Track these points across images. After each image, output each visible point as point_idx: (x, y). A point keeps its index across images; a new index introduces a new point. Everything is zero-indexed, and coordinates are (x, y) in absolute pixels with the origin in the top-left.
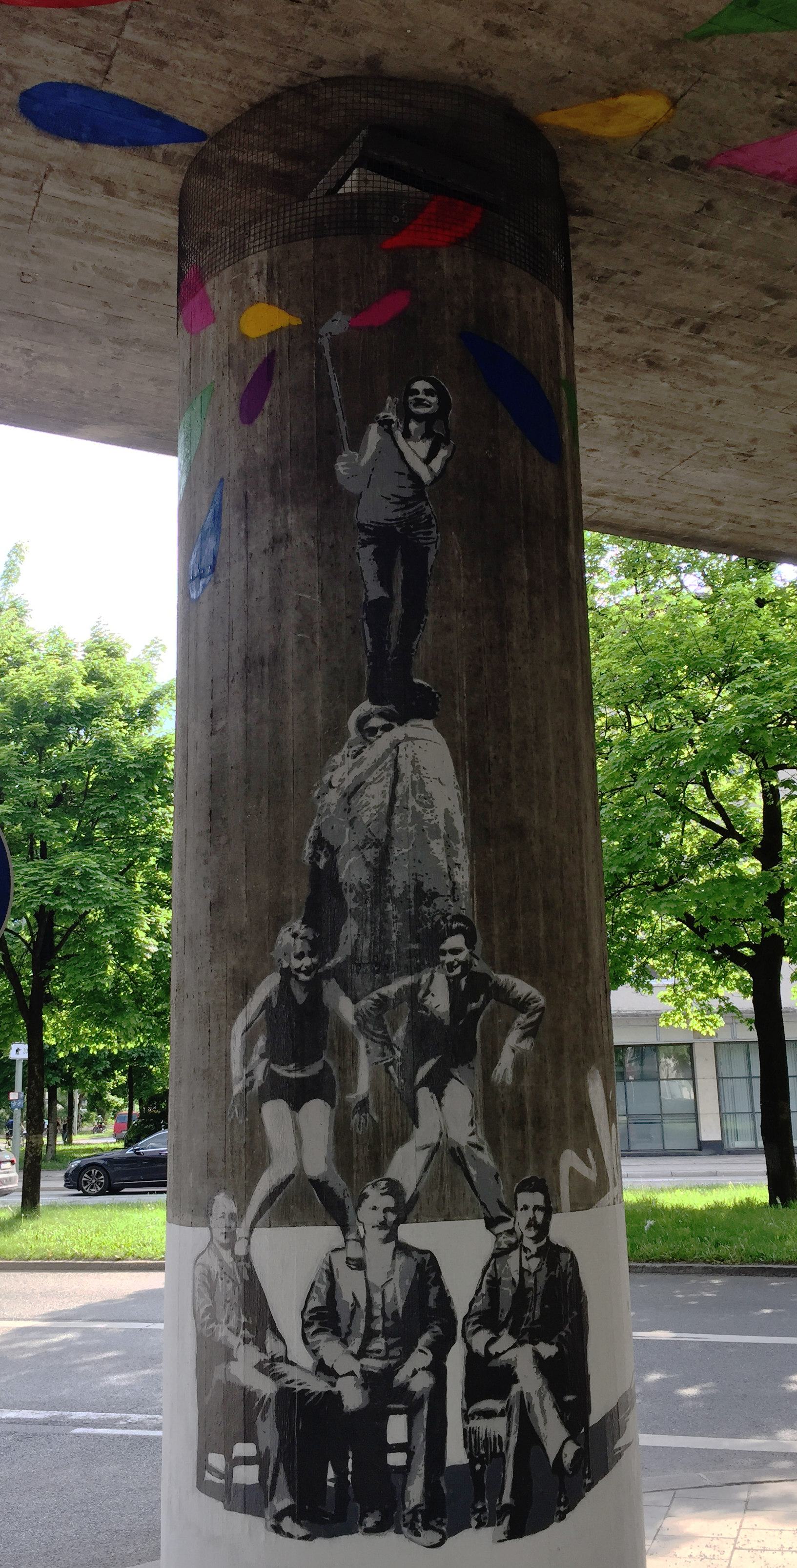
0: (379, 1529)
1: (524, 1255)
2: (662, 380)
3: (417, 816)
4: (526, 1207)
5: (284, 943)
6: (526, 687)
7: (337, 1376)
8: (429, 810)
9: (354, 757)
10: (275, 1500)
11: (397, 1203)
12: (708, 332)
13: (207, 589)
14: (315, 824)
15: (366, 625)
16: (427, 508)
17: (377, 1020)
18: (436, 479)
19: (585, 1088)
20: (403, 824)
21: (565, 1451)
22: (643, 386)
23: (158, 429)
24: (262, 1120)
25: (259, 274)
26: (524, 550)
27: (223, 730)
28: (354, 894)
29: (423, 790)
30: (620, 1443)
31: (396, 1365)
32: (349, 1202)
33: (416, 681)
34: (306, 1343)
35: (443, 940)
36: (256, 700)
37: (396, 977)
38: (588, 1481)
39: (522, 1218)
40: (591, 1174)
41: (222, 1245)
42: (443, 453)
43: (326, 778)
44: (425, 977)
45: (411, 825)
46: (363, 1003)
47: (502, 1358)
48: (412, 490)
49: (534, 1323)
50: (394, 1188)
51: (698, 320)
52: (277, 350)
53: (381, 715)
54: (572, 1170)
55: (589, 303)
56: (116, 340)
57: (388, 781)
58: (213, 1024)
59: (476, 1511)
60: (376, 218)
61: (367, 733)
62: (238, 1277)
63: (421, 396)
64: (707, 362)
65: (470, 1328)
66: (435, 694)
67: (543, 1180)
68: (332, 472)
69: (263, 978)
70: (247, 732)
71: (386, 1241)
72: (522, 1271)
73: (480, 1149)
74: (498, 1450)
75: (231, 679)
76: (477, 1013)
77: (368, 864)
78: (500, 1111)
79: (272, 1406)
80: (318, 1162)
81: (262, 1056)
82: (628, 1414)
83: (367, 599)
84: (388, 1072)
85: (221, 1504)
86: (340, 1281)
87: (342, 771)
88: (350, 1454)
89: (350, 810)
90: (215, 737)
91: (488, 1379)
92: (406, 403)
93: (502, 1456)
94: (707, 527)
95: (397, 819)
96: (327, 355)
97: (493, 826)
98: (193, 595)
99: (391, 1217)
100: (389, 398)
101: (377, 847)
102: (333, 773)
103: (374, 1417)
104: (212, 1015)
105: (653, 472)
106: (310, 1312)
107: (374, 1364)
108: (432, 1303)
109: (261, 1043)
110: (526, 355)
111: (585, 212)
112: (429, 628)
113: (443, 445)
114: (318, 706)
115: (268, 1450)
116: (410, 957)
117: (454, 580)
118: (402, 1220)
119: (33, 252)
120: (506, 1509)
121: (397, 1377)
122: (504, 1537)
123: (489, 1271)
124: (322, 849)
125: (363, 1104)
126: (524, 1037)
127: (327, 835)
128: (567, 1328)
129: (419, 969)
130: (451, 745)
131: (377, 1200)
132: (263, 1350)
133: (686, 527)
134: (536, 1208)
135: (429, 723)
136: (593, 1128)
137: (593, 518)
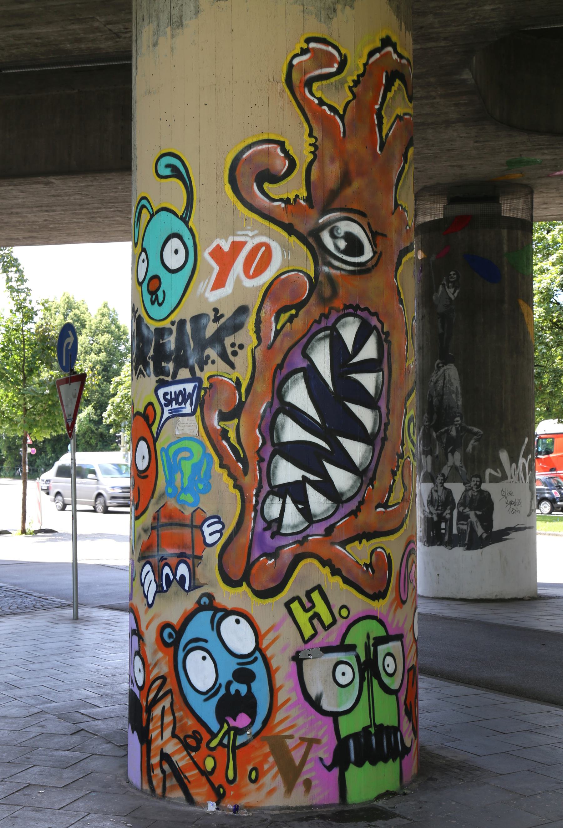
17: (439, 438)
32: (435, 478)
39: (473, 484)
42: (457, 291)
44: (450, 428)
50: (443, 475)
53: (442, 363)
61: (439, 368)
72: (472, 495)
87: (434, 379)
91: (462, 517)
95: (445, 389)
107: (439, 512)
118: (445, 482)
120: (466, 544)
125: (437, 457)
126: (475, 442)
130: (458, 370)
131: (440, 479)
134: (477, 481)
135: (452, 365)
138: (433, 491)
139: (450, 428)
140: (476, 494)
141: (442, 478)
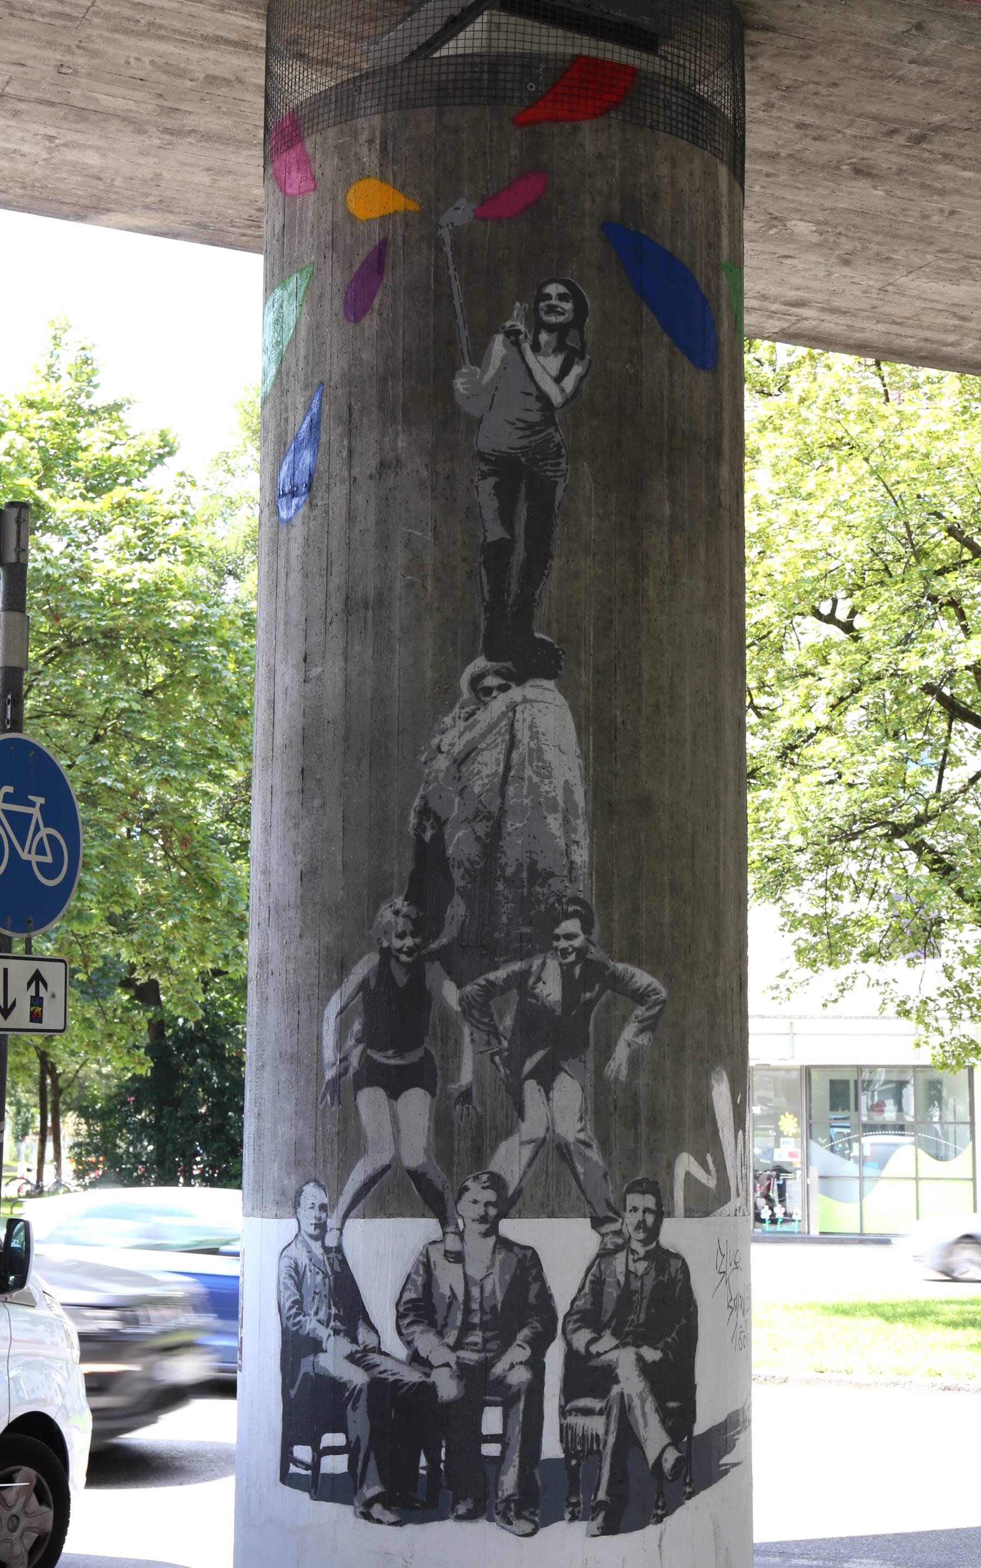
0: (471, 1516)
1: (631, 1257)
2: (875, 188)
3: (534, 788)
4: (635, 1209)
5: (385, 920)
6: (661, 641)
7: (432, 1367)
8: (546, 781)
9: (467, 719)
10: (365, 1489)
11: (499, 1196)
12: (931, 142)
13: (301, 511)
14: (421, 792)
15: (483, 571)
16: (557, 435)
17: (479, 1009)
18: (567, 402)
19: (709, 1089)
20: (518, 795)
21: (666, 1455)
22: (851, 193)
23: (206, 220)
24: (356, 1107)
25: (370, 142)
26: (666, 480)
27: (319, 678)
28: (462, 871)
29: (540, 759)
30: (727, 1459)
31: (494, 1358)
32: (449, 1196)
33: (538, 635)
34: (400, 1333)
35: (557, 924)
36: (358, 648)
37: (505, 962)
38: (688, 1490)
39: (631, 1220)
40: (710, 1182)
41: (311, 1236)
42: (577, 370)
43: (435, 741)
44: (536, 963)
45: (526, 797)
46: (468, 988)
47: (603, 1358)
48: (540, 414)
49: (638, 1325)
50: (496, 1182)
51: (916, 131)
52: (390, 239)
53: (498, 673)
54: (688, 1174)
55: (775, 111)
56: (166, 131)
57: (503, 747)
58: (303, 1005)
59: (570, 1505)
60: (509, 85)
61: (481, 693)
62: (328, 1269)
63: (554, 302)
64: (932, 171)
65: (570, 1327)
66: (557, 650)
67: (656, 1183)
68: (449, 390)
69: (360, 957)
70: (347, 684)
71: (486, 1235)
72: (628, 1273)
73: (589, 1146)
74: (595, 1447)
75: (329, 620)
76: (590, 1004)
77: (478, 839)
78: (612, 1107)
79: (364, 1396)
80: (415, 1154)
81: (358, 1041)
82: (738, 1433)
83: (485, 540)
84: (493, 1062)
85: (307, 1495)
86: (437, 1273)
87: (453, 737)
88: (444, 1443)
89: (460, 778)
90: (308, 686)
91: (587, 1378)
92: (536, 311)
93: (599, 1453)
94: (952, 345)
95: (511, 790)
96: (447, 249)
97: (618, 800)
98: (284, 514)
99: (493, 1212)
100: (518, 304)
101: (489, 820)
102: (443, 736)
103: (469, 1408)
104: (302, 995)
105: (871, 283)
106: (406, 1303)
107: (470, 1356)
108: (532, 1299)
109: (357, 1026)
110: (679, 244)
111: (766, 28)
112: (554, 575)
113: (577, 359)
114: (429, 659)
115: (358, 1440)
116: (521, 941)
117: (584, 519)
118: (503, 1214)
119: (78, 47)
120: (600, 1505)
121: (493, 1370)
122: (597, 1532)
123: (593, 1271)
124: (428, 820)
125: (466, 1095)
126: (641, 1031)
127: (434, 804)
128: (674, 1335)
129: (530, 955)
130: (574, 709)
131: (475, 1199)
132: (354, 1340)
133: (922, 344)
134: (646, 1210)
135: (550, 684)
136: (716, 1132)
137: (791, 330)
138: (436, 1256)
139: (536, 963)
140: (641, 1267)
141: (491, 1195)
